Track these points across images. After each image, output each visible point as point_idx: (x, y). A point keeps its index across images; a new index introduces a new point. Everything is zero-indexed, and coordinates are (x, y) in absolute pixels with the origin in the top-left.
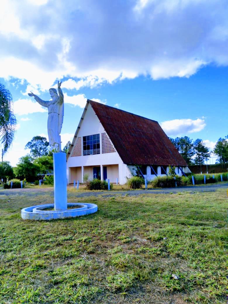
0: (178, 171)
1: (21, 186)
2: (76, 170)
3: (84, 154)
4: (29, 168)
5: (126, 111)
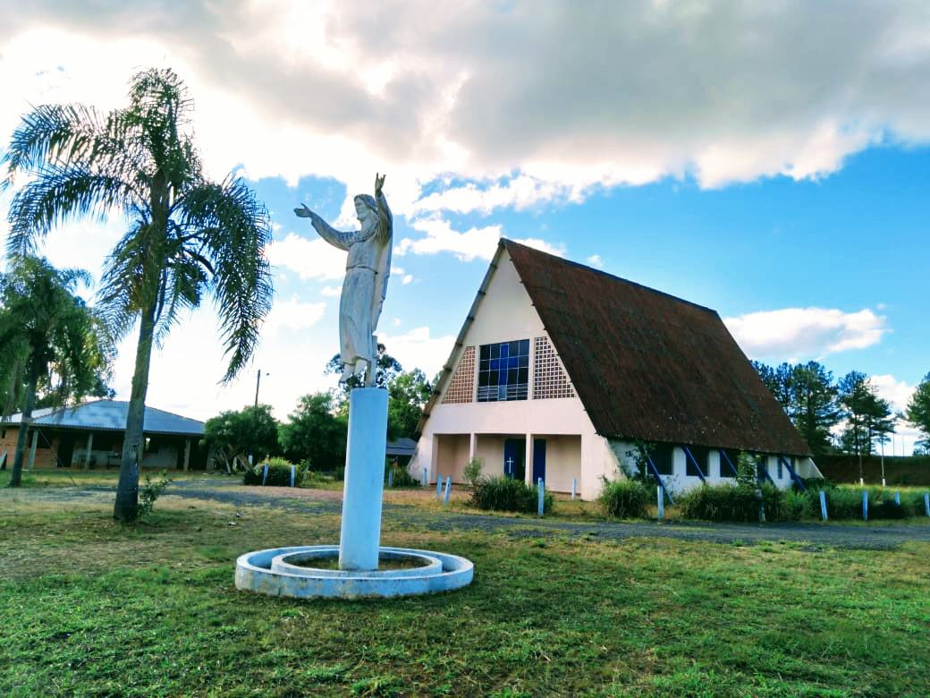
0: (780, 471)
1: (290, 480)
2: (452, 443)
4: (321, 428)
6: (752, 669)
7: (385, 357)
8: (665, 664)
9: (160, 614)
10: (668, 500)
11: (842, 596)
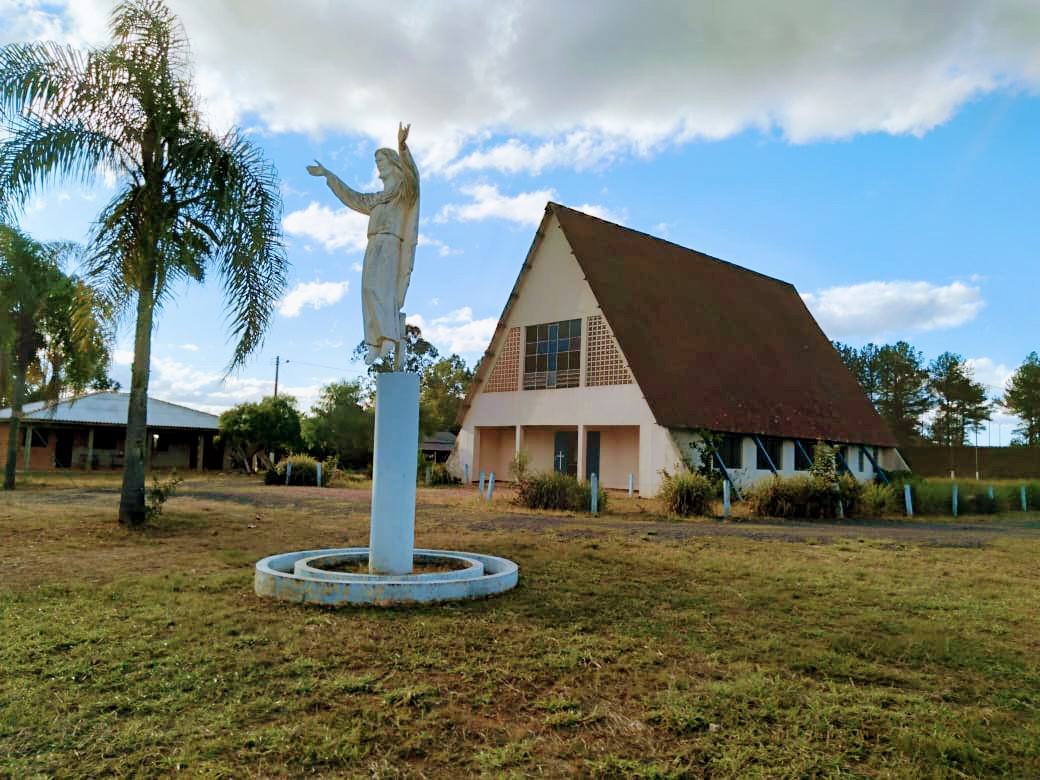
2: (495, 437)
3: (525, 384)
9: (172, 624)
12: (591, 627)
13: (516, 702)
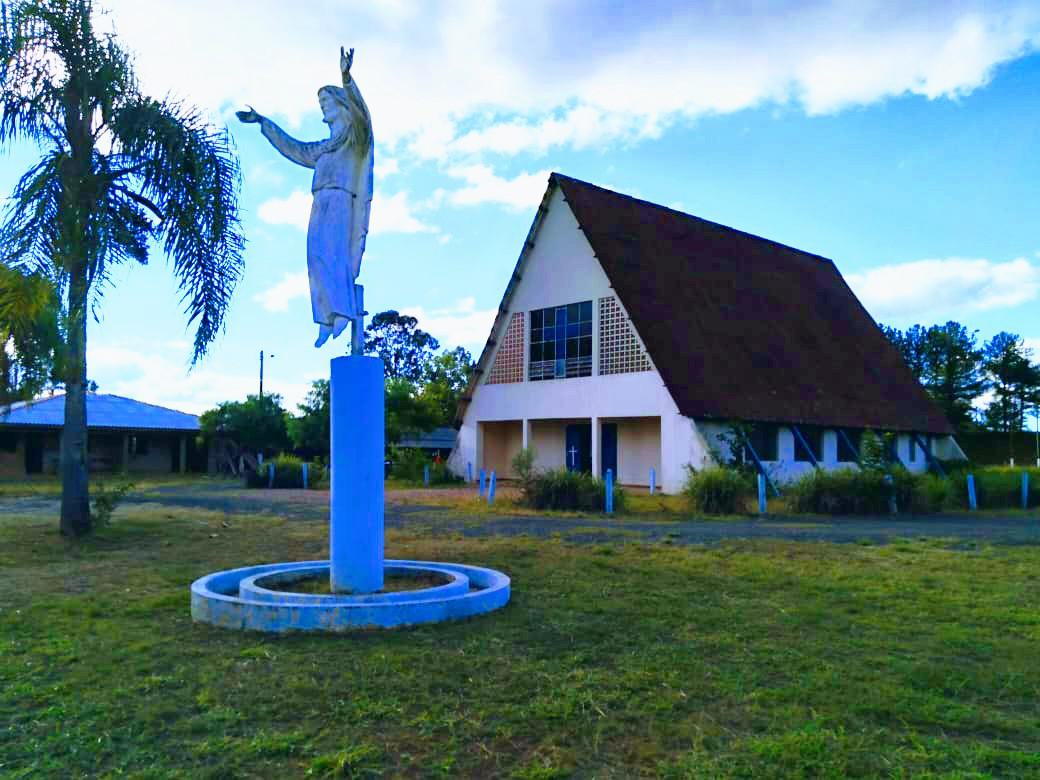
2: (500, 432)
3: (530, 374)
5: (734, 227)
6: (899, 722)
7: (417, 332)
8: (771, 716)
9: (75, 660)
10: (773, 491)
11: (1013, 608)
12: (595, 658)
13: (487, 768)
